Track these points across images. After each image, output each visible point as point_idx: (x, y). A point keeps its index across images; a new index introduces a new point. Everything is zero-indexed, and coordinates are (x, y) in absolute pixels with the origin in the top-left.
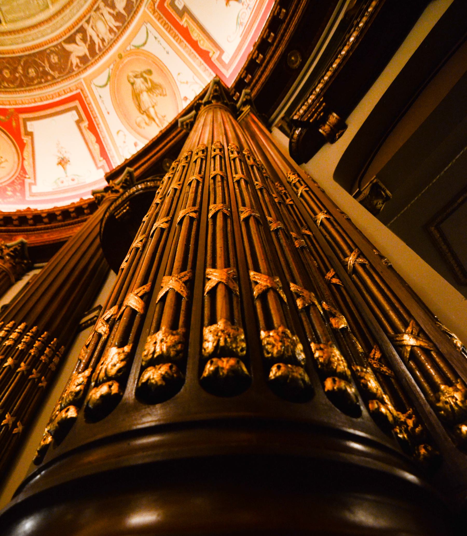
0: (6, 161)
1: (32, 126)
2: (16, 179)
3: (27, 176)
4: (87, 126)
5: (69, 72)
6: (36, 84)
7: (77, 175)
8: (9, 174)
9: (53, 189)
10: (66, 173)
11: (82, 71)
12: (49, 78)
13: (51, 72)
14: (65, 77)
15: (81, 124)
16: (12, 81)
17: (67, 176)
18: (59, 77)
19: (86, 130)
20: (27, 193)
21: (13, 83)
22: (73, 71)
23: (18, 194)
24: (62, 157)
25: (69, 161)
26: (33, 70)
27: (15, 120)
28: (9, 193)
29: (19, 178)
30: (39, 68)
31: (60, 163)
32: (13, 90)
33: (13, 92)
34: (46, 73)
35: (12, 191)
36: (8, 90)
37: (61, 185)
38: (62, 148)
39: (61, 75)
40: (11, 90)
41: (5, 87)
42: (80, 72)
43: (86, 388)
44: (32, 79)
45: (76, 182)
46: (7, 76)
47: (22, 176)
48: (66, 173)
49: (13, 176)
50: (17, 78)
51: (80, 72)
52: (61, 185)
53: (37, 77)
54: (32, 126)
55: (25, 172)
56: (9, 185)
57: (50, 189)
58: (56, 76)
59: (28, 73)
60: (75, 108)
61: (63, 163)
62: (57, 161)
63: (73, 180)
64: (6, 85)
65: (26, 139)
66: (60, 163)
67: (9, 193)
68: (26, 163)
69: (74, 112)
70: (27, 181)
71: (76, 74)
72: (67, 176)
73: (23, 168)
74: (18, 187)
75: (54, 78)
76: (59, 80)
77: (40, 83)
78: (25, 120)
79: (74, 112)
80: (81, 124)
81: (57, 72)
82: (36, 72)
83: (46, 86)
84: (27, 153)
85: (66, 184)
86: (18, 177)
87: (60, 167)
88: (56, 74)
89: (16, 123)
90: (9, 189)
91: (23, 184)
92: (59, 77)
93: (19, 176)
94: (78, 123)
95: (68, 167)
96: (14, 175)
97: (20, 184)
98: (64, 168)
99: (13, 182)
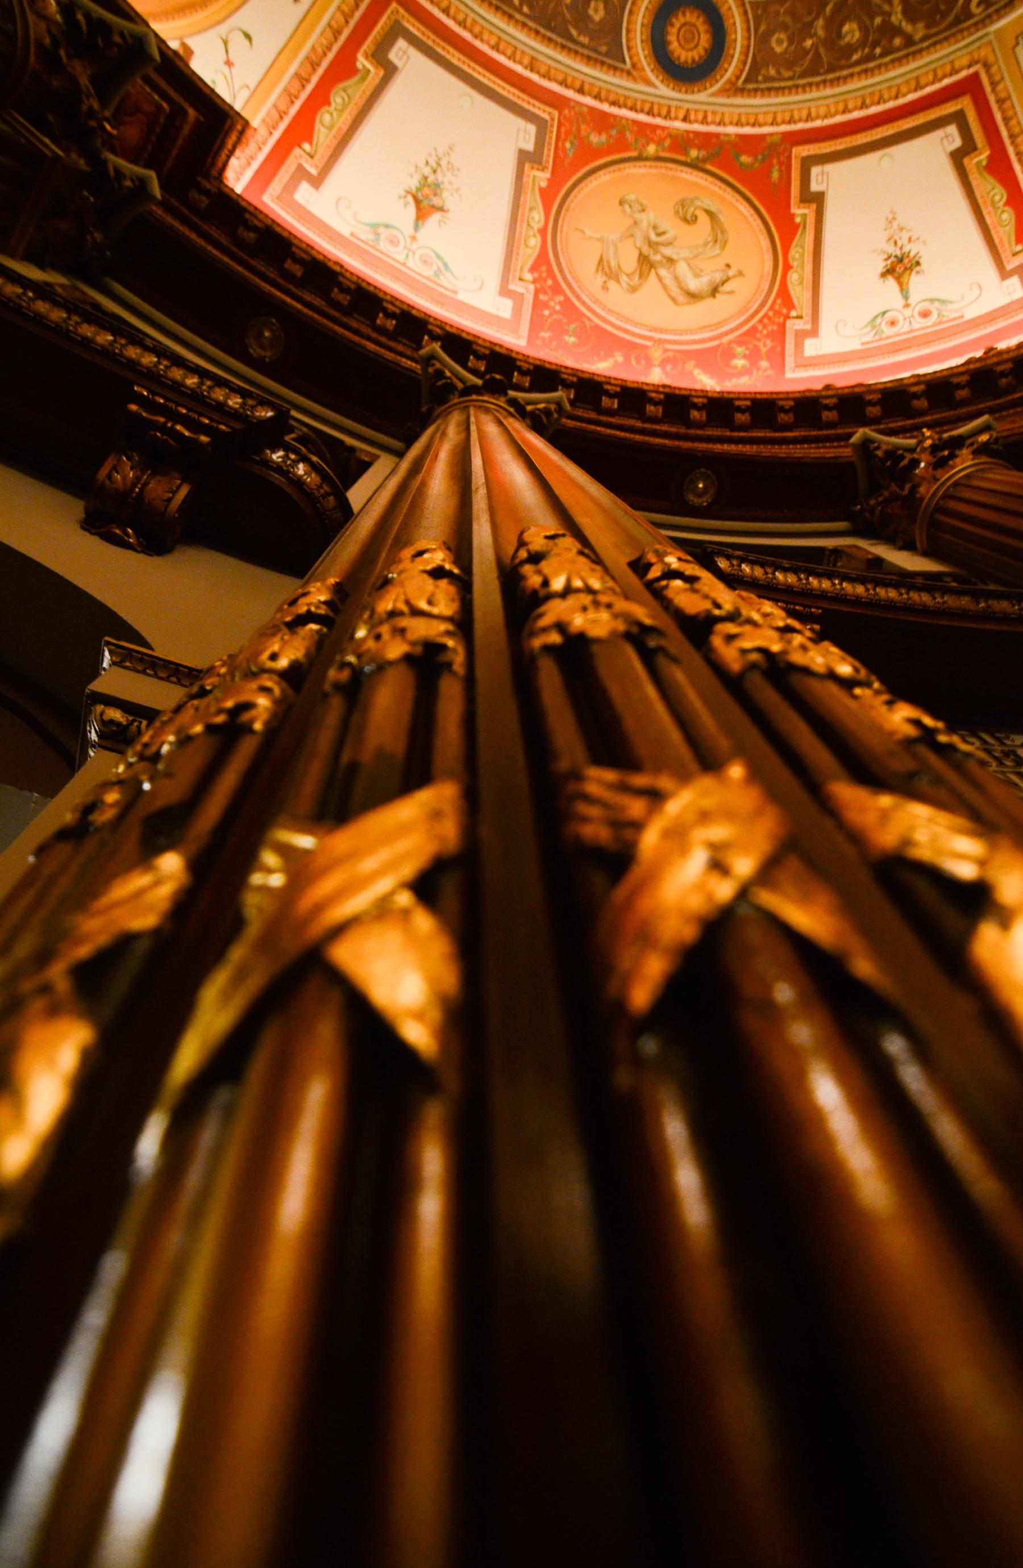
0: (740, 274)
1: (820, 178)
2: (761, 321)
3: (793, 313)
4: (984, 163)
5: (957, 22)
6: (858, 63)
7: (939, 300)
8: (741, 312)
9: (352, 234)
10: (906, 297)
11: (997, 11)
12: (897, 42)
13: (907, 27)
14: (942, 36)
15: (966, 161)
16: (788, 62)
17: (907, 306)
18: (924, 39)
19: (980, 174)
20: (789, 360)
21: (790, 65)
22: (969, 15)
23: (764, 364)
24: (899, 253)
25: (918, 264)
26: (855, 26)
27: (780, 163)
28: (739, 363)
29: (769, 319)
30: (872, 19)
31: (889, 272)
32: (790, 83)
33: (790, 88)
34: (890, 30)
35: (745, 357)
36: (776, 85)
37: (888, 331)
38: (902, 229)
39: (934, 30)
40: (783, 84)
41: (768, 79)
42: (989, 16)
43: (223, 381)
44: (851, 49)
45: (934, 318)
46: (778, 49)
47: (778, 313)
48: (906, 297)
49: (752, 316)
50: (806, 52)
51: (989, 16)
52: (888, 331)
53: (862, 43)
54: (820, 178)
55: (789, 303)
56: (740, 342)
57: (855, 345)
58: (918, 36)
59: (840, 36)
60: (542, 126)
61: (899, 269)
62: (881, 266)
63: (925, 314)
64: (772, 72)
65: (800, 212)
66: (889, 272)
67: (739, 363)
68: (793, 277)
69: (952, 129)
70: (793, 326)
71: (976, 24)
72: (907, 306)
73: (784, 293)
74: (765, 346)
75: (909, 41)
76: (925, 44)
77: (870, 58)
78: (808, 163)
79: (532, 129)
80: (966, 161)
81: (920, 26)
82: (864, 29)
83: (886, 65)
84: (800, 251)
85: (903, 327)
86: (766, 315)
87: (891, 282)
88: (918, 31)
89: (780, 171)
90: (739, 350)
91: (780, 335)
92: (924, 39)
93: (771, 313)
94: (958, 158)
95: (914, 281)
96: (757, 312)
97: (770, 335)
98: (901, 285)
99: (752, 332)
